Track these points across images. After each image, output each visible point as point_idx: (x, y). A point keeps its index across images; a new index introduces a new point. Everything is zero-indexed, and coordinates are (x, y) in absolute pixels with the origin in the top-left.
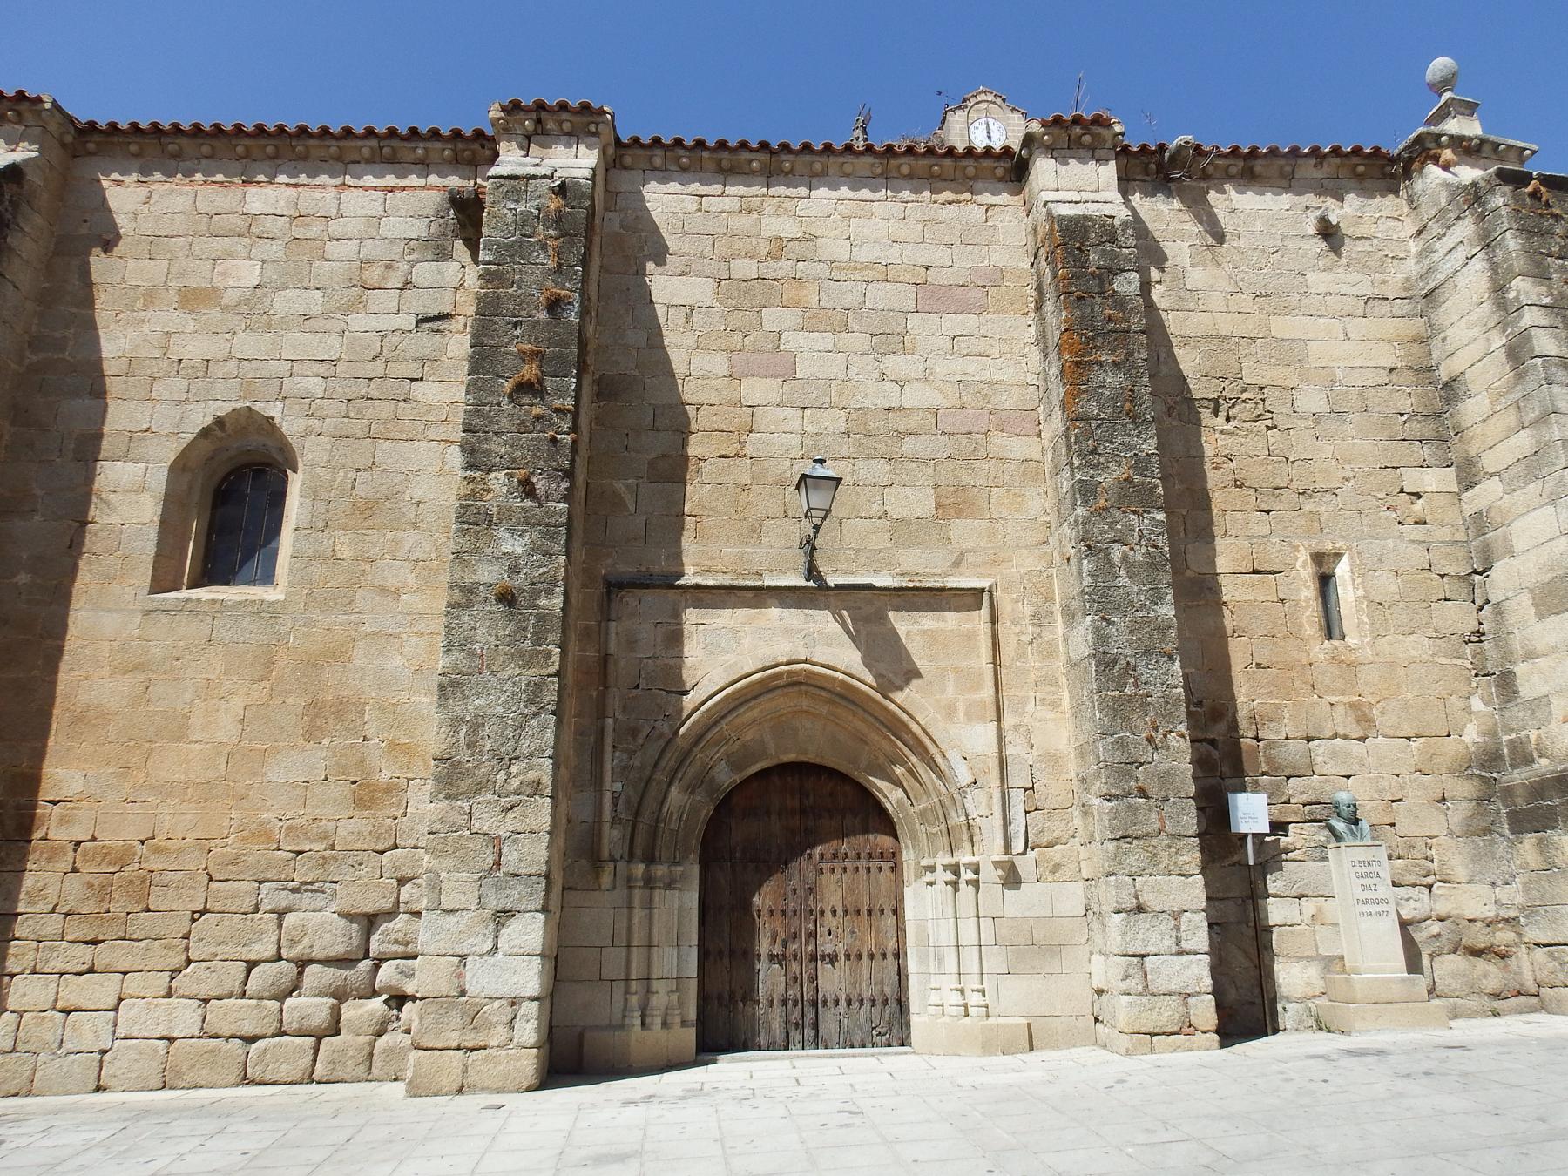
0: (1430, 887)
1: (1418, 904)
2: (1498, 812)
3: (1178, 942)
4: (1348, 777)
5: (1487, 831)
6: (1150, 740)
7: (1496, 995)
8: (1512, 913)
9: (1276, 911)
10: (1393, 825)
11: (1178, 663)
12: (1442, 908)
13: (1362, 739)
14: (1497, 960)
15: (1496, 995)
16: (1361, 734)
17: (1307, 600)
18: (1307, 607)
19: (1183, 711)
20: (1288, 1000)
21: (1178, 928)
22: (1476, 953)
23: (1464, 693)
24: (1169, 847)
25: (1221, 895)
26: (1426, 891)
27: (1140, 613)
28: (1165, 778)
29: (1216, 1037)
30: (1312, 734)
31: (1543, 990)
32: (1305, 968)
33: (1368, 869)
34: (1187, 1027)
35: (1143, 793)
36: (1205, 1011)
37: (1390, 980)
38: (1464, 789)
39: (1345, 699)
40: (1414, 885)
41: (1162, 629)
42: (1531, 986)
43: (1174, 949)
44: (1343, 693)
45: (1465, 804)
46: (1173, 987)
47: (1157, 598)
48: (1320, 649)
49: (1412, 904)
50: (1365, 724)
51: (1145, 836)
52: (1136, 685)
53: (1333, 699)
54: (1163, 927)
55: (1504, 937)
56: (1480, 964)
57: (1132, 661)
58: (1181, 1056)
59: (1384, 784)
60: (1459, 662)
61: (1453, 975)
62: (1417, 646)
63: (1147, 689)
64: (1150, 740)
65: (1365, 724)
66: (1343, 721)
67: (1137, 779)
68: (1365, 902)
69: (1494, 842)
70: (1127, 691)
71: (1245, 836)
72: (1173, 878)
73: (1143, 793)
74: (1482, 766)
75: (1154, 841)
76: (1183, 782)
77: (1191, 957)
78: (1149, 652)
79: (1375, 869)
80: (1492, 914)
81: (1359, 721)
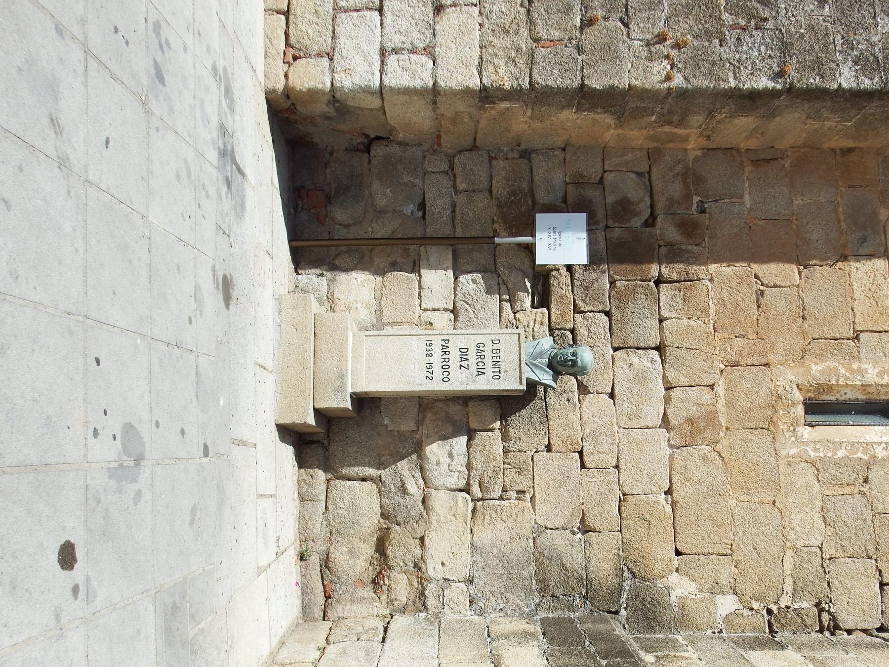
0: (467, 489)
1: (444, 468)
2: (571, 608)
3: (396, 51)
4: (612, 395)
5: (543, 586)
6: (661, 38)
7: (326, 563)
8: (431, 602)
9: (437, 281)
10: (549, 448)
11: (771, 85)
12: (440, 500)
13: (665, 422)
14: (372, 574)
15: (326, 563)
16: (674, 421)
17: (861, 372)
18: (853, 372)
19: (703, 82)
20: (332, 281)
21: (414, 51)
22: (381, 547)
23: (741, 587)
24: (518, 50)
25: (458, 216)
26: (462, 484)
27: (839, 40)
28: (610, 53)
29: (280, 86)
30: (670, 353)
31: (328, 624)
32: (368, 306)
33: (488, 360)
34: (294, 54)
35: (588, 23)
36: (311, 76)
37: (343, 358)
38: (601, 559)
39: (721, 407)
40: (469, 466)
41: (818, 66)
42: (338, 610)
43: (389, 46)
44: (730, 405)
45: (579, 558)
46: (343, 42)
47: (864, 64)
48: (790, 379)
49: (445, 460)
50: (689, 432)
51: (531, 22)
52: (735, 26)
53: (720, 390)
54: (416, 35)
55: (401, 585)
56: (368, 549)
57: (770, 25)
58: (259, 43)
59: (605, 444)
60: (789, 588)
61: (354, 507)
62: (807, 527)
63: (731, 40)
64: (661, 38)
65: (689, 432)
66: (686, 404)
67: (606, 19)
68: (445, 351)
69: (529, 593)
70: (726, 16)
71: (533, 235)
72: (476, 52)
73: (588, 23)
74: (635, 596)
75: (524, 32)
76: (606, 73)
77: (377, 65)
78: (785, 48)
79: (489, 370)
80: (431, 572)
81: (691, 421)
